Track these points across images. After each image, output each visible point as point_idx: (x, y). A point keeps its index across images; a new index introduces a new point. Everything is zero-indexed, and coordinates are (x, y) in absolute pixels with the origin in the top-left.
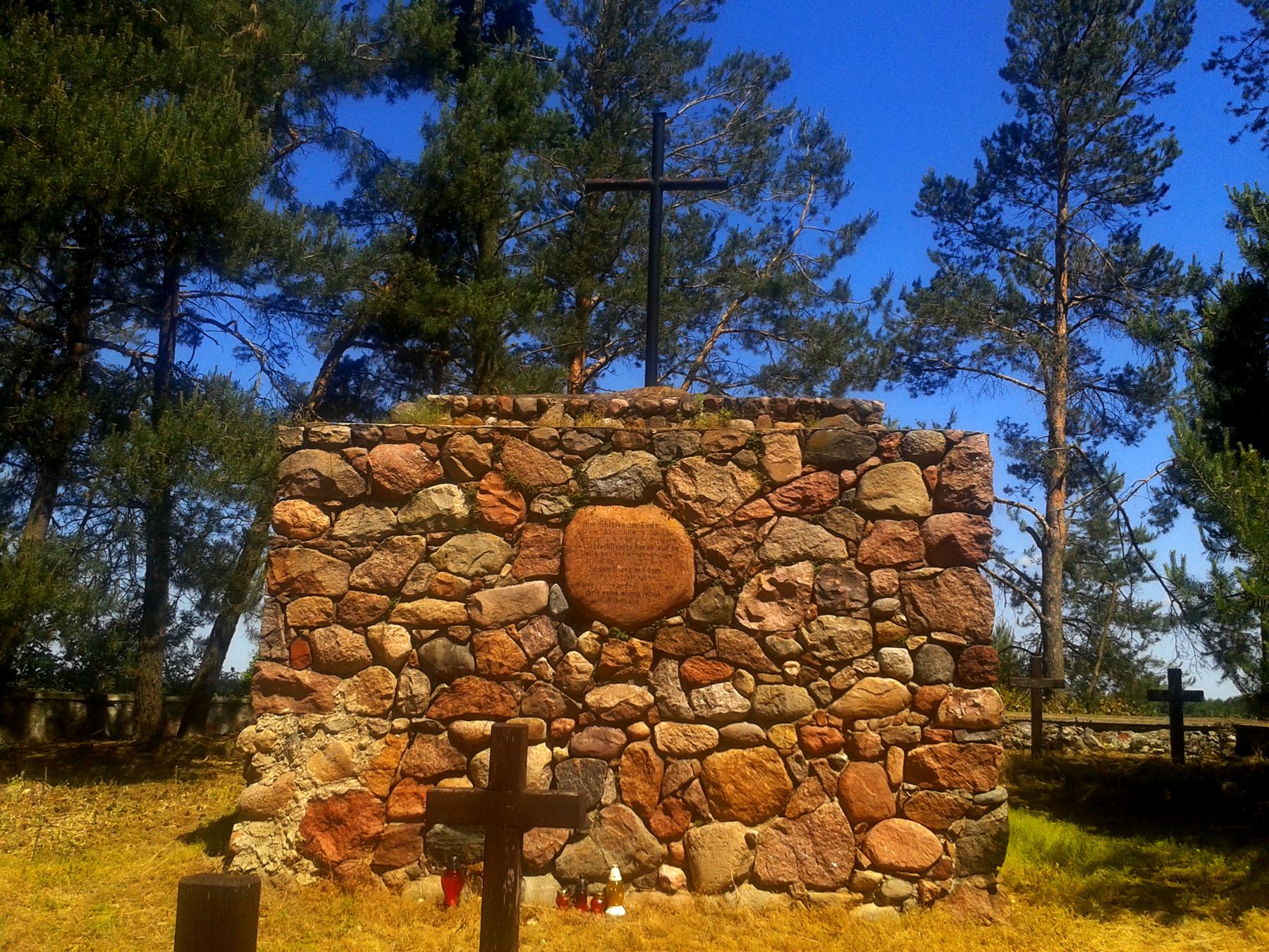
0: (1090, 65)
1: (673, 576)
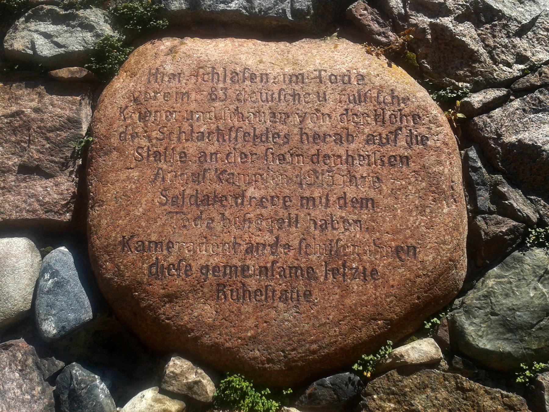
0: (484, 43)
1: (414, 219)
